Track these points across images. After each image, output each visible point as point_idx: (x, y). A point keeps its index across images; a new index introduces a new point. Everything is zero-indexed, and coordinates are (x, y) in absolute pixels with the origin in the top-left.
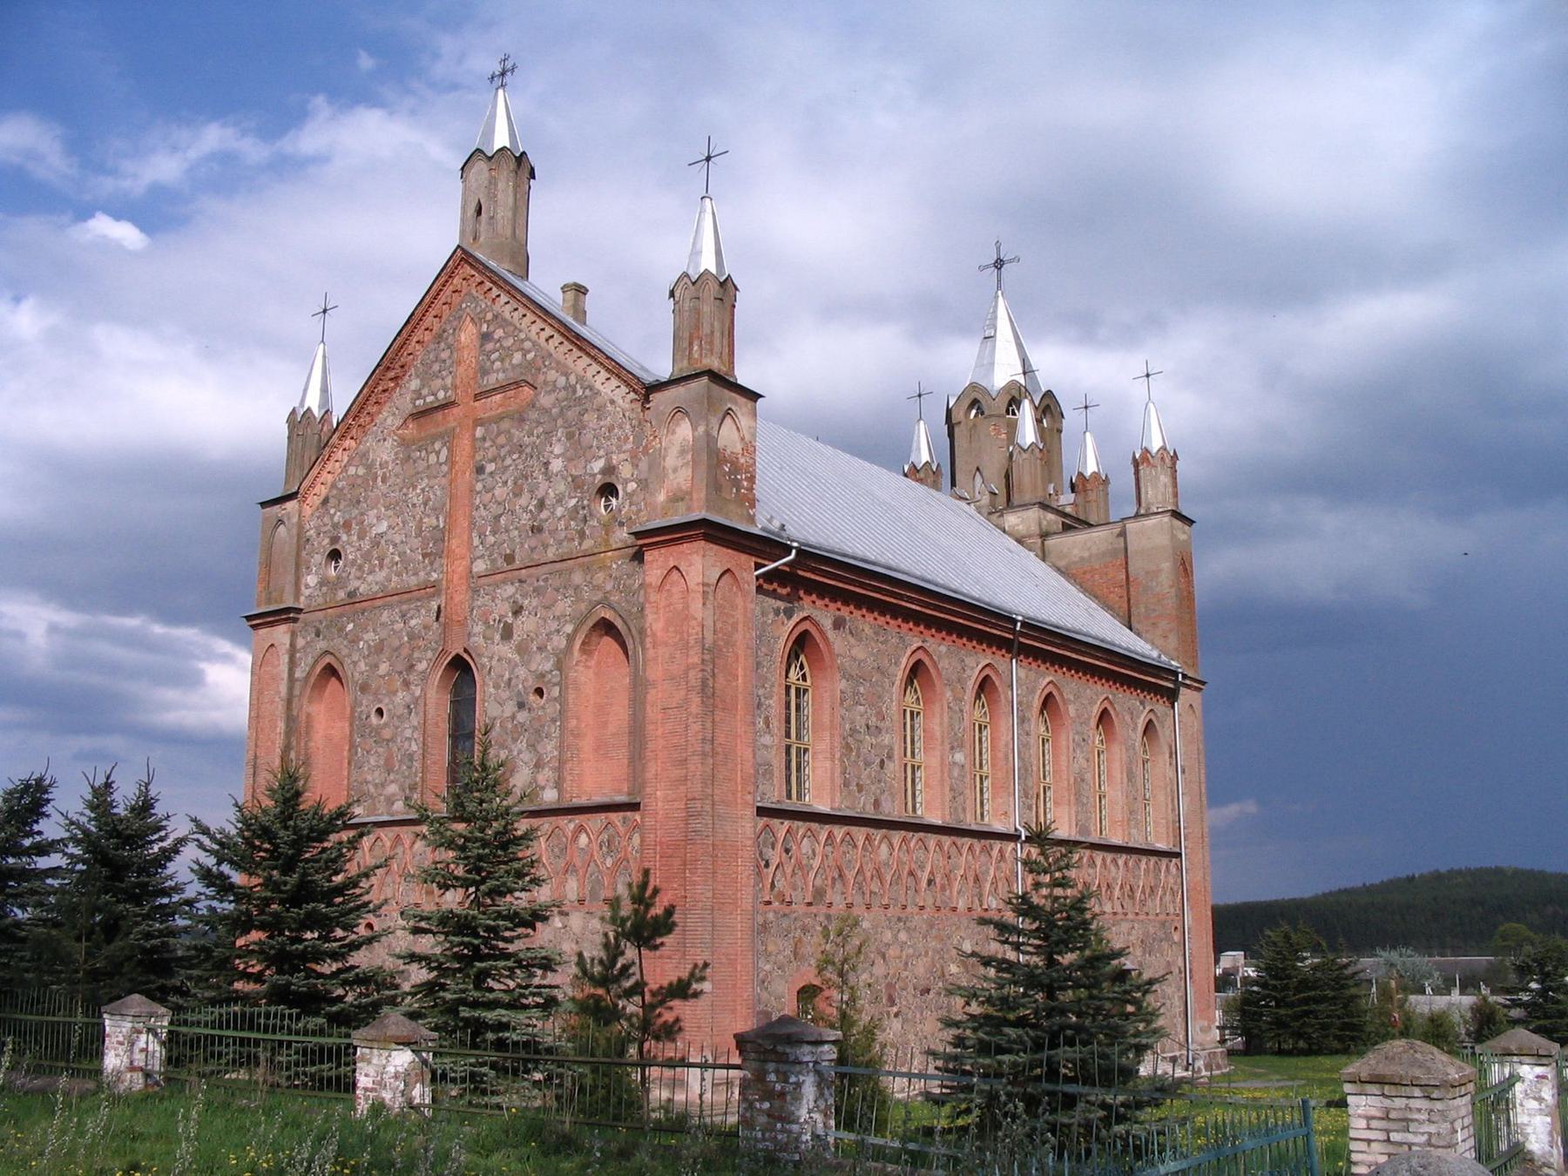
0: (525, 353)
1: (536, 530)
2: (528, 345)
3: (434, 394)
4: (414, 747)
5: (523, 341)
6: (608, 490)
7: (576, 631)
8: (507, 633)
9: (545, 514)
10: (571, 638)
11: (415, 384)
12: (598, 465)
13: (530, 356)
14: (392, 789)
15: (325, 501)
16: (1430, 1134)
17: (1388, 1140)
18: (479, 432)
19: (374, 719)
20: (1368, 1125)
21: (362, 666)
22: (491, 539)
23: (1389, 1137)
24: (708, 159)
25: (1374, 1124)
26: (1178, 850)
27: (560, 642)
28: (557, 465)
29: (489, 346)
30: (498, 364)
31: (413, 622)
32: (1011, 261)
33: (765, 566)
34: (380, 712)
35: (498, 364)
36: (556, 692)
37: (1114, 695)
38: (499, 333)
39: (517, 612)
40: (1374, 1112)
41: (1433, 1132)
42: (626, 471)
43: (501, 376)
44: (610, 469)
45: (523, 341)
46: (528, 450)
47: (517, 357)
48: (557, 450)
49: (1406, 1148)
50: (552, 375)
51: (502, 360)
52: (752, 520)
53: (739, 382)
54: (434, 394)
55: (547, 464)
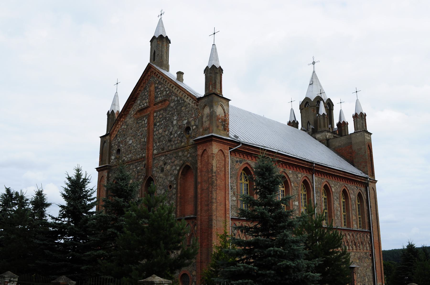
1: (170, 141)
3: (144, 105)
6: (188, 129)
8: (162, 170)
10: (179, 171)
11: (139, 102)
12: (185, 122)
13: (168, 92)
15: (117, 135)
22: (158, 144)
26: (232, 202)
27: (176, 172)
28: (175, 122)
30: (160, 95)
31: (138, 168)
32: (317, 62)
33: (232, 148)
36: (175, 186)
37: (347, 185)
38: (160, 87)
39: (165, 164)
42: (193, 123)
43: (161, 98)
44: (188, 123)
46: (168, 119)
47: (165, 93)
48: (175, 118)
51: (161, 94)
52: (228, 135)
54: (144, 105)
55: (172, 122)
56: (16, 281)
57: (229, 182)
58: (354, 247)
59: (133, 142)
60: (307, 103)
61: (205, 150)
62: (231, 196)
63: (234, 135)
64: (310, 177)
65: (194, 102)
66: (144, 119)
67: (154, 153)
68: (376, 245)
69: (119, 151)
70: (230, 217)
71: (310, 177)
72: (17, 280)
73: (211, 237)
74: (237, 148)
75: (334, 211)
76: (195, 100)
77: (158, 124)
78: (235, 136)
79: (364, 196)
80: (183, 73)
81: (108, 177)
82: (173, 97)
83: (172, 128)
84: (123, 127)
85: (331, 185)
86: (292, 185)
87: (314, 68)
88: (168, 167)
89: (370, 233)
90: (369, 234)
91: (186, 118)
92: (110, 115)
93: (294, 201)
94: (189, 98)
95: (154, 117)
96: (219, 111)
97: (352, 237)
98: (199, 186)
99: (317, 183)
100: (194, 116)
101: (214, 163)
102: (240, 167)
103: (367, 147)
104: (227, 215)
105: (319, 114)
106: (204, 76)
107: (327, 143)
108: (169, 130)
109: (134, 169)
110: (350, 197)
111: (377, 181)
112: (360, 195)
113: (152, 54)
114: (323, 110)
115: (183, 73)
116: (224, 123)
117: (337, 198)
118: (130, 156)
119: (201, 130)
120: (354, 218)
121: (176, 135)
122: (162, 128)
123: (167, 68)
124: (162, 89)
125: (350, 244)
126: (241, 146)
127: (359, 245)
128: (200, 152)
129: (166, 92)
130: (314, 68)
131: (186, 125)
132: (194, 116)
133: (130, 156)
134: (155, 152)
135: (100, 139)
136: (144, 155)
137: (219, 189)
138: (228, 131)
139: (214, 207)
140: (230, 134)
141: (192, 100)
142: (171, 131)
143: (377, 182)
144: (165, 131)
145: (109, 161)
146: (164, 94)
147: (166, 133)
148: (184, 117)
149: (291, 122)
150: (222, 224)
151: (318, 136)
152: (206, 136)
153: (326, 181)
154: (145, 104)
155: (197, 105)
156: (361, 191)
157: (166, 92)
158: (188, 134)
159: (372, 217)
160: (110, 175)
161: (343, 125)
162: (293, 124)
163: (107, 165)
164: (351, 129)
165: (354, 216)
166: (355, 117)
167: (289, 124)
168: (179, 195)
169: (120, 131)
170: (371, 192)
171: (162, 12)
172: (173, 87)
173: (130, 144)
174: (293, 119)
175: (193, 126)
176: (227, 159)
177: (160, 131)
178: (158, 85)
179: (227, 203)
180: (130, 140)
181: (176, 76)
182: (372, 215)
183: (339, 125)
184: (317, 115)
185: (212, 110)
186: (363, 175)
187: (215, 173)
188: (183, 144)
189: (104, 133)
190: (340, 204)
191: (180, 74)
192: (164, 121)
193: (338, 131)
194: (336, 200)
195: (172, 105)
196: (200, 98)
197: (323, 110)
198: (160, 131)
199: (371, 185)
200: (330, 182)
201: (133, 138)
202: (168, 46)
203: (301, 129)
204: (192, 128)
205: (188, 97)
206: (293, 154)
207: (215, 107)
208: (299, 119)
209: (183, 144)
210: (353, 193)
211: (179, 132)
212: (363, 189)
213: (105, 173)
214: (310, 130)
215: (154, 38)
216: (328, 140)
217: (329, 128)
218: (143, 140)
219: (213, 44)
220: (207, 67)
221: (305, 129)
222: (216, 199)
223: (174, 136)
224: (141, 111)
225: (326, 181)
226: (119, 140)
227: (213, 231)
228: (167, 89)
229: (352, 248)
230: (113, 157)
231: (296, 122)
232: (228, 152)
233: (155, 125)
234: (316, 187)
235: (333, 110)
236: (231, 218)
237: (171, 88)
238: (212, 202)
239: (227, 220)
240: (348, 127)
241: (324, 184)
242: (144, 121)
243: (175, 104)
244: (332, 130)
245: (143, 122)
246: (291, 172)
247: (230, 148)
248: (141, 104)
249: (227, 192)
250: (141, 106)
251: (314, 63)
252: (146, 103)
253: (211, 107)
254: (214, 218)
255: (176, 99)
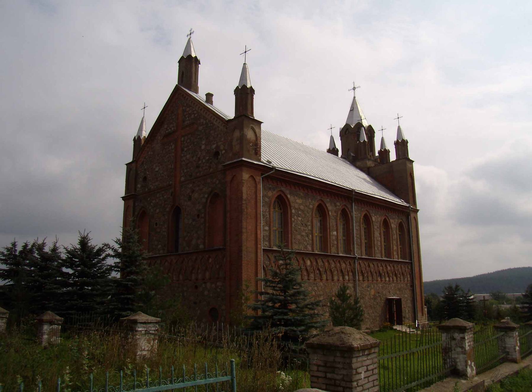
0: (195, 114)
1: (198, 167)
2: (195, 112)
3: (171, 129)
4: (165, 234)
5: (194, 111)
6: (217, 154)
7: (208, 197)
8: (190, 198)
9: (200, 162)
10: (207, 199)
11: (166, 126)
12: (214, 146)
13: (196, 115)
14: (160, 246)
15: (143, 163)
16: (344, 375)
17: (325, 377)
18: (183, 139)
19: (155, 226)
20: (318, 369)
21: (152, 210)
22: (185, 171)
23: (326, 376)
24: (245, 52)
25: (321, 369)
26: (264, 232)
27: (204, 200)
28: (203, 147)
29: (185, 113)
30: (187, 118)
31: (165, 197)
32: (358, 87)
33: (264, 174)
34: (156, 224)
35: (187, 118)
36: (203, 215)
37: (388, 214)
38: (188, 109)
39: (193, 191)
40: (320, 363)
41: (345, 374)
42: (222, 147)
43: (188, 122)
44: (218, 147)
45: (194, 111)
46: (195, 143)
47: (193, 116)
48: (203, 142)
49: (333, 381)
50: (202, 120)
51: (188, 117)
52: (259, 160)
53: (255, 118)
54: (171, 129)
55: (200, 147)
56: (6, 318)
57: (261, 211)
58: (395, 278)
59: (159, 169)
60: (347, 129)
61: (235, 175)
62: (263, 226)
63: (267, 160)
64: (349, 206)
65: (223, 125)
66: (172, 144)
67: (181, 180)
68: (417, 275)
69: (145, 179)
70: (262, 248)
71: (349, 206)
72: (8, 317)
73: (241, 269)
74: (270, 174)
75: (374, 241)
76: (224, 123)
77: (185, 149)
78: (268, 161)
79: (405, 226)
80: (212, 95)
81: (134, 207)
82: (202, 120)
83: (200, 153)
84: (149, 153)
85: (371, 214)
86: (330, 214)
87: (354, 94)
88: (196, 195)
89: (411, 263)
90: (410, 265)
91: (215, 142)
92: (137, 141)
93: (332, 230)
94: (218, 121)
95: (181, 141)
96: (250, 134)
97: (393, 268)
98: (228, 215)
99: (356, 212)
100: (223, 139)
101: (244, 190)
102: (273, 194)
103: (409, 174)
104: (259, 246)
105: (360, 142)
106: (234, 97)
107: (368, 171)
108: (196, 156)
109: (161, 198)
110: (391, 226)
111: (419, 210)
112: (401, 226)
113: (181, 73)
114: (364, 137)
115: (212, 95)
116: (255, 147)
117: (378, 228)
118: (157, 184)
119: (231, 155)
120: (395, 248)
121: (204, 161)
122: (189, 154)
123: (196, 91)
124: (190, 112)
125: (391, 275)
126: (273, 173)
127: (399, 276)
128: (229, 178)
129: (194, 115)
130: (354, 94)
131: (214, 150)
132: (223, 139)
133: (157, 184)
134: (183, 179)
135: (126, 166)
136: (171, 182)
137: (249, 217)
138: (260, 155)
139: (244, 237)
140: (262, 159)
141: (221, 123)
142: (198, 156)
143: (419, 211)
144: (193, 157)
145: (135, 190)
146: (192, 117)
147: (194, 159)
148: (212, 141)
149: (331, 149)
150: (253, 256)
151: (358, 164)
152: (235, 161)
153: (366, 210)
154: (173, 129)
155: (227, 128)
156: (403, 221)
157: (194, 115)
158: (217, 159)
159: (414, 247)
160: (136, 204)
161: (385, 153)
162: (333, 151)
163: (133, 193)
164: (393, 157)
165: (395, 247)
166: (397, 144)
167: (329, 151)
168: (207, 225)
169: (146, 157)
170: (413, 221)
171: (192, 32)
172: (201, 110)
173: (157, 171)
174: (333, 146)
175: (221, 151)
176: (258, 186)
177: (188, 156)
178: (186, 108)
179: (259, 232)
180: (156, 166)
181: (204, 98)
182: (414, 246)
183: (380, 152)
184: (358, 142)
185: (242, 133)
186: (405, 204)
187: (245, 200)
188: (211, 170)
189: (130, 159)
190: (380, 234)
191: (209, 96)
192: (192, 145)
193: (380, 159)
194: (376, 229)
195: (201, 128)
196: (230, 121)
197: (364, 137)
198: (188, 156)
199: (412, 215)
200: (371, 211)
201: (159, 165)
202: (197, 67)
203: (342, 157)
204: (221, 153)
205: (217, 120)
206: (322, 178)
207: (245, 130)
208: (338, 145)
209: (211, 170)
210: (394, 222)
211: (207, 158)
212: (404, 219)
213: (131, 202)
214: (351, 158)
215: (182, 57)
216: (369, 168)
217: (371, 156)
218: (170, 166)
219: (244, 63)
220: (238, 87)
221: (346, 157)
222: (246, 228)
223: (202, 161)
224: (167, 136)
225: (366, 210)
226: (146, 167)
227: (243, 262)
228: (195, 112)
229: (393, 279)
230: (139, 186)
231: (336, 149)
232: (259, 179)
233: (182, 150)
234: (355, 217)
235: (374, 137)
236: (263, 249)
237: (199, 111)
238: (241, 232)
239: (259, 251)
240: (389, 155)
241: (364, 213)
242: (172, 146)
243: (203, 127)
244: (374, 158)
245: (170, 148)
246: (328, 200)
247: (262, 174)
248: (168, 128)
249: (259, 221)
250: (168, 130)
251: (354, 89)
252: (173, 127)
253: (242, 129)
254: (244, 248)
255: (205, 122)
